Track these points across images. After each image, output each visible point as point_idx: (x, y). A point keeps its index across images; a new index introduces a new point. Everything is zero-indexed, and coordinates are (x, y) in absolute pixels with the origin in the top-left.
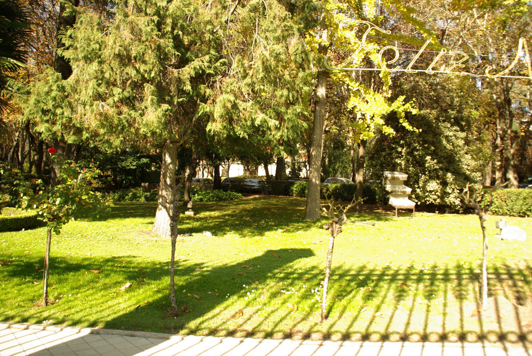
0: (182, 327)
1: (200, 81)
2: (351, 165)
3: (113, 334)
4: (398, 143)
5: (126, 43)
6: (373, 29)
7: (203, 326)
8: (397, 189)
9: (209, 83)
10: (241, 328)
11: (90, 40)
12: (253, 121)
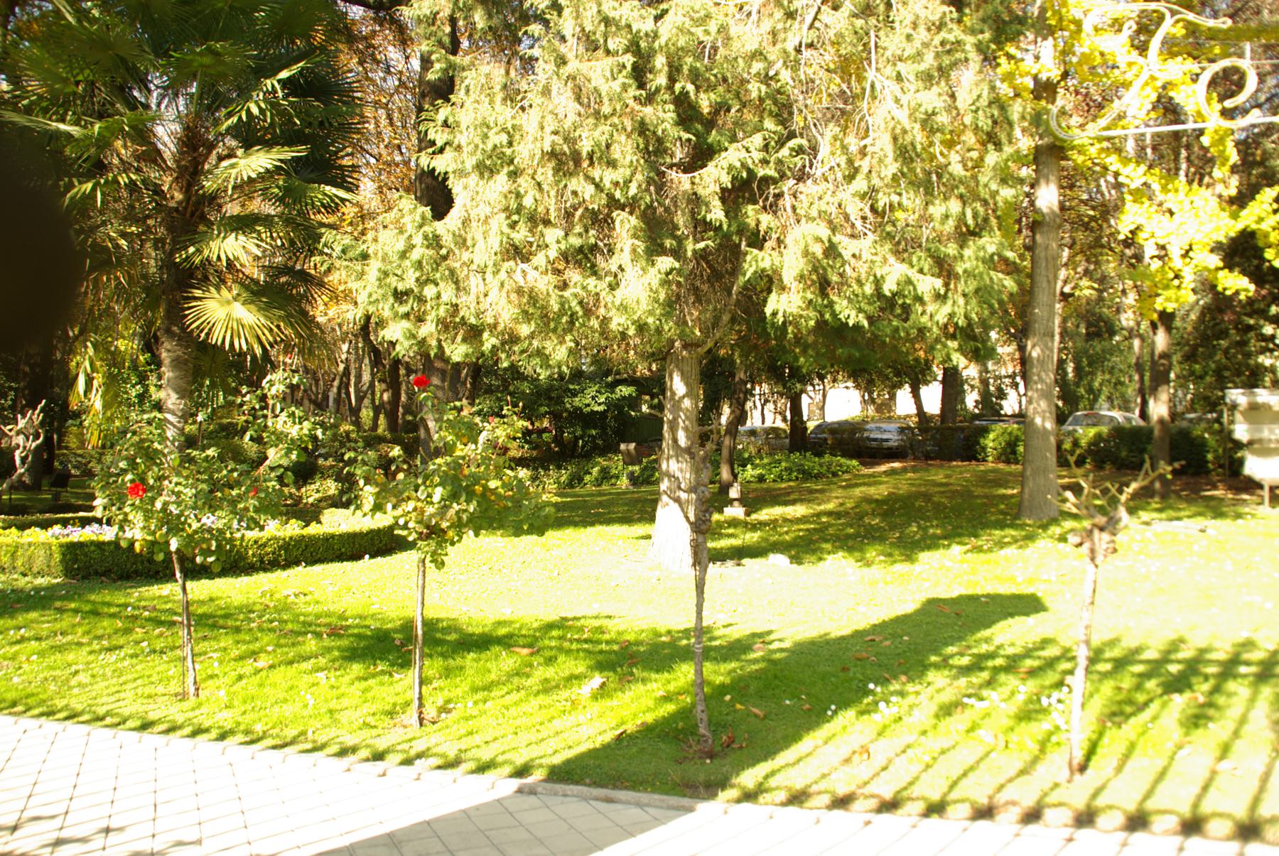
0: (723, 784)
1: (744, 197)
2: (1136, 377)
3: (565, 795)
4: (1263, 313)
5: (568, 124)
6: (1177, 21)
7: (772, 782)
8: (1265, 434)
9: (767, 198)
10: (868, 790)
11: (488, 127)
12: (878, 283)
